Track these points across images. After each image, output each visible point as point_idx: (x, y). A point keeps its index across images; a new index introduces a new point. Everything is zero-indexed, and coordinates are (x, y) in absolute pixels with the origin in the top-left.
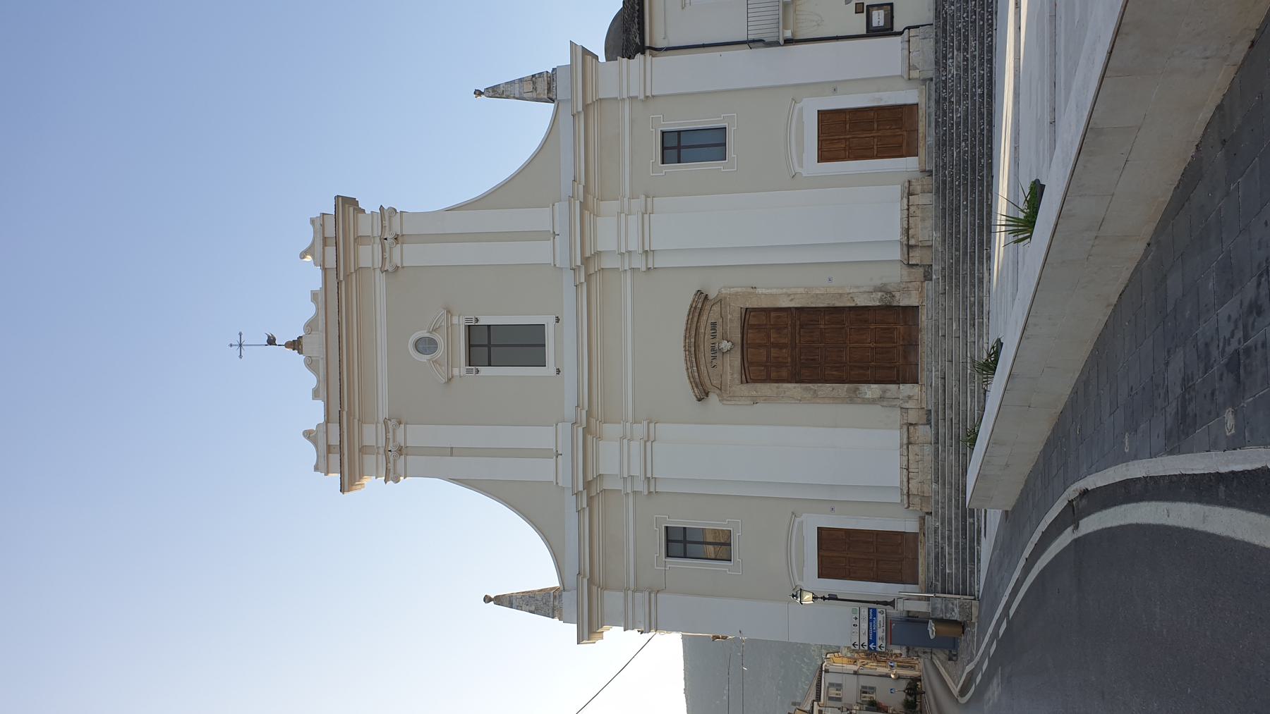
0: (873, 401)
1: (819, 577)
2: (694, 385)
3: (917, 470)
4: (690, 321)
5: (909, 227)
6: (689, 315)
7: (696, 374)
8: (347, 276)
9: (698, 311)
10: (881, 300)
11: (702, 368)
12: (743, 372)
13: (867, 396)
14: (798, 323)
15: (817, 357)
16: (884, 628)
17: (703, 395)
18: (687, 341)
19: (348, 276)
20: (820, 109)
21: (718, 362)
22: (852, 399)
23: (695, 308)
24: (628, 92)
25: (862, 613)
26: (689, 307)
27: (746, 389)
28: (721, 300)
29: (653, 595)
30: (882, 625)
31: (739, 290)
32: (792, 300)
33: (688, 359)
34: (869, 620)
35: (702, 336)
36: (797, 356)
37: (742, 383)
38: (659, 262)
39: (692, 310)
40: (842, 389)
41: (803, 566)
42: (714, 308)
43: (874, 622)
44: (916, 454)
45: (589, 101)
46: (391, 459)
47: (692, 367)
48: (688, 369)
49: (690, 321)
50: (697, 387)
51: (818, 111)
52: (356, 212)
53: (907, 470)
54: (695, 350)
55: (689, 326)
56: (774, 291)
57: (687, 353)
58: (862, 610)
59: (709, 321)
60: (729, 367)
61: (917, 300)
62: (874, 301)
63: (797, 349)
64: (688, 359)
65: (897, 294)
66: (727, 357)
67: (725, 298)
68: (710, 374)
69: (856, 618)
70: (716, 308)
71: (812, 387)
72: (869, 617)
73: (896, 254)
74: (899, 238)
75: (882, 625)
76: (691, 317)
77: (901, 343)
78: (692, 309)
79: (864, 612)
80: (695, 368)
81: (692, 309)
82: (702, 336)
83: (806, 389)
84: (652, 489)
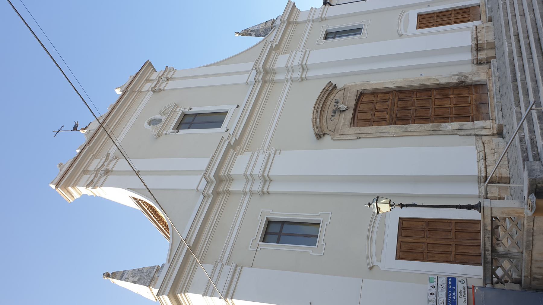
0: (452, 133)
1: (396, 259)
2: (315, 126)
3: (494, 159)
4: (321, 96)
5: (477, 36)
6: (321, 93)
7: (318, 122)
8: (133, 91)
9: (328, 92)
10: (458, 79)
11: (323, 121)
12: (353, 122)
13: (448, 129)
14: (397, 98)
15: (409, 114)
16: (466, 297)
17: (320, 136)
18: (317, 105)
19: (133, 91)
20: (402, 216)
21: (336, 117)
22: (435, 133)
23: (327, 90)
24: (313, 16)
25: (440, 281)
26: (323, 89)
27: (353, 130)
28: (345, 89)
29: (239, 268)
30: (463, 294)
31: (358, 83)
32: (394, 84)
33: (315, 114)
34: (448, 289)
35: (328, 106)
36: (394, 114)
37: (350, 127)
38: (310, 74)
39: (324, 91)
40: (428, 126)
41: (383, 249)
42: (339, 92)
43: (454, 291)
44: (492, 149)
45: (291, 20)
46: (99, 175)
47: (316, 118)
48: (313, 118)
49: (321, 96)
50: (317, 128)
51: (400, 218)
52: (153, 71)
53: (485, 159)
54: (321, 111)
55: (320, 98)
56: (382, 81)
57: (315, 111)
58: (440, 280)
59: (335, 99)
60: (343, 119)
61: (486, 77)
62: (455, 80)
63: (395, 111)
64: (315, 114)
65: (470, 76)
66: (343, 115)
67: (348, 87)
68: (327, 121)
69: (433, 287)
70: (341, 93)
71: (404, 126)
72: (448, 285)
73: (469, 56)
74: (470, 44)
75: (463, 294)
76: (323, 94)
77: (474, 103)
78: (325, 91)
79: (442, 281)
80: (318, 119)
81: (325, 91)
82: (328, 106)
83: (399, 127)
84: (265, 190)
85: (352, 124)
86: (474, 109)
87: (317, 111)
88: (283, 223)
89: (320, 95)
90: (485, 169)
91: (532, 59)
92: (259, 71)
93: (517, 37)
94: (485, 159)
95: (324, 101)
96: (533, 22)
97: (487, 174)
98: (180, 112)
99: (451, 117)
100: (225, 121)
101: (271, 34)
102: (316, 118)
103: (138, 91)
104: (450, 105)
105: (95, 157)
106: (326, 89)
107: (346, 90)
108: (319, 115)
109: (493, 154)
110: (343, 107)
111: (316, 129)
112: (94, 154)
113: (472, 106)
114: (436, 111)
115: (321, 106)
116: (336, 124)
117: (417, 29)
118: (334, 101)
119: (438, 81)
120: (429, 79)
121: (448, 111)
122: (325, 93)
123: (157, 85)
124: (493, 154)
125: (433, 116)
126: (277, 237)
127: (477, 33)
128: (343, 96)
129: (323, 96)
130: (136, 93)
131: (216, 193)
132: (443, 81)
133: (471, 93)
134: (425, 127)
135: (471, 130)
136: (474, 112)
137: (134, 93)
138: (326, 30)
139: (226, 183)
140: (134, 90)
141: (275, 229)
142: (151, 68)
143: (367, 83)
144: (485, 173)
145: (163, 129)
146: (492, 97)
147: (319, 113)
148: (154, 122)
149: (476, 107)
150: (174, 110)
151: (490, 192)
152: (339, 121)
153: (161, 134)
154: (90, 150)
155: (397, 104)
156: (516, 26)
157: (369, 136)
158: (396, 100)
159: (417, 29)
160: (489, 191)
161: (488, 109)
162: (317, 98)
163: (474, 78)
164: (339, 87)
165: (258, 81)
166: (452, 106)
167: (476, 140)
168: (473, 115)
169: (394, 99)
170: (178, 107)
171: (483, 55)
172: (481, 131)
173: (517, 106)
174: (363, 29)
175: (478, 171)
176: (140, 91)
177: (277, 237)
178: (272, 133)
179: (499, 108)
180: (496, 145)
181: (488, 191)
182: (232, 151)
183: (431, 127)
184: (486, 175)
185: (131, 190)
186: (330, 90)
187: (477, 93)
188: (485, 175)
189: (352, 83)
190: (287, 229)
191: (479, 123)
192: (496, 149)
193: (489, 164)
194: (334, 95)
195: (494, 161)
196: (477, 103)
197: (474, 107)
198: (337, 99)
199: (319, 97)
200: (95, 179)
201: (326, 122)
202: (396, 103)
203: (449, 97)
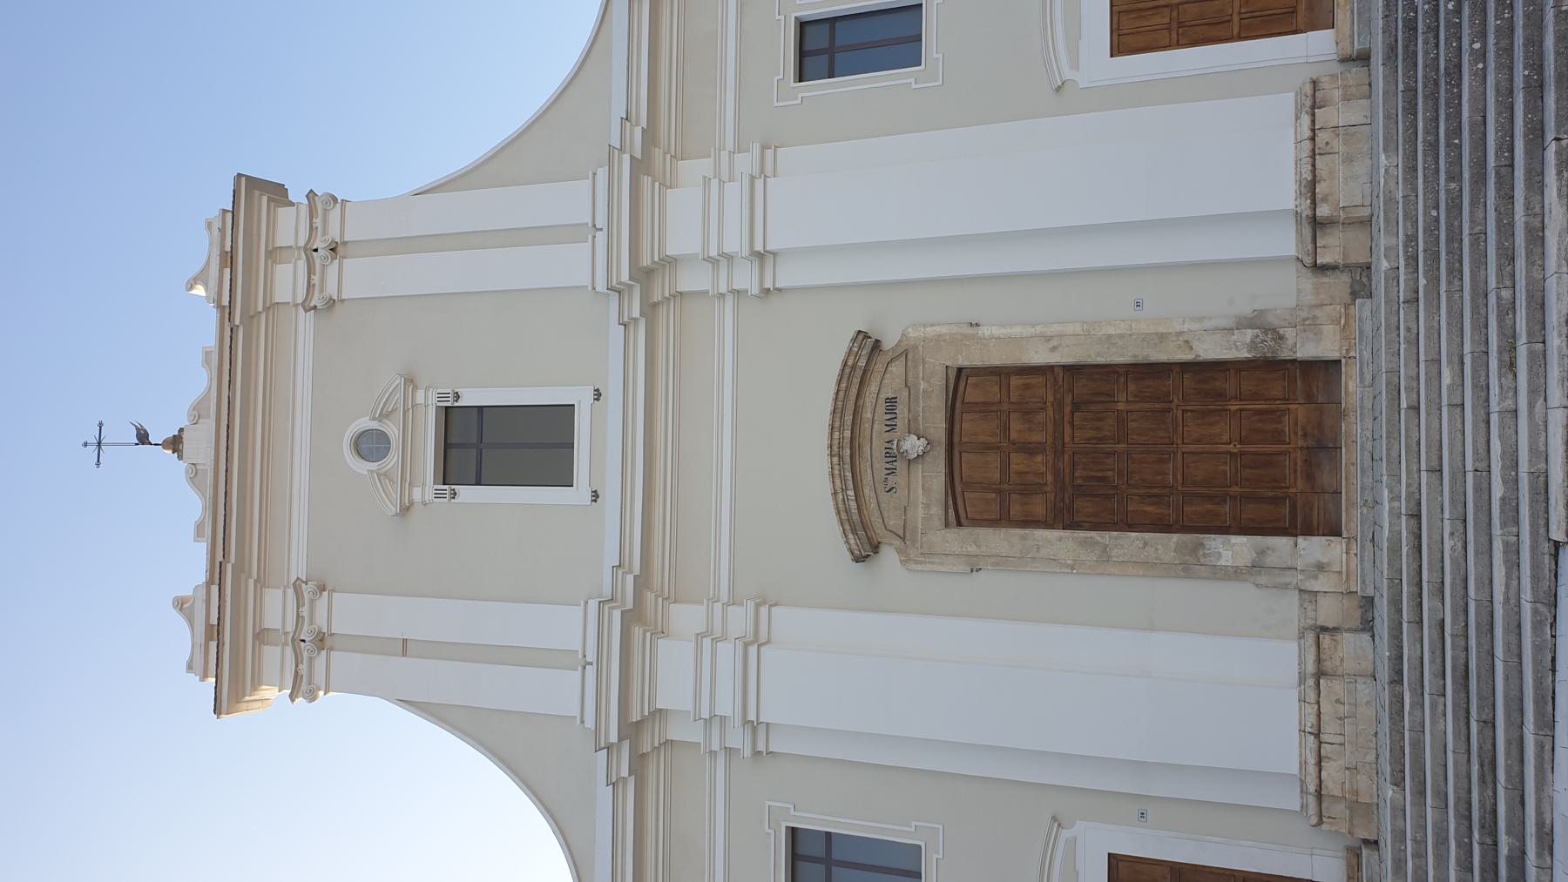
0: (1235, 574)
2: (847, 527)
3: (1339, 739)
8: (250, 318)
9: (859, 373)
10: (1253, 345)
13: (1222, 562)
14: (1068, 399)
17: (866, 549)
18: (836, 434)
19: (252, 317)
21: (899, 480)
22: (1188, 568)
23: (854, 367)
26: (839, 367)
28: (906, 353)
31: (944, 330)
32: (1054, 349)
33: (837, 472)
39: (847, 371)
40: (1167, 544)
44: (1337, 701)
47: (844, 490)
50: (854, 532)
52: (272, 204)
53: (1317, 736)
56: (1017, 331)
57: (836, 459)
63: (1066, 457)
65: (1289, 333)
66: (918, 472)
70: (897, 369)
73: (1286, 242)
78: (847, 370)
80: (851, 493)
84: (761, 747)
85: (950, 511)
86: (1299, 469)
87: (840, 457)
88: (832, 21)
89: (837, 393)
90: (1317, 769)
91: (1442, 699)
92: (627, 563)
93: (1413, 522)
94: (1317, 736)
95: (852, 412)
96: (1457, 581)
97: (1323, 786)
98: (430, 407)
99: (1233, 498)
100: (578, 461)
101: (608, 13)
102: (844, 490)
103: (267, 309)
104: (1230, 443)
105: (261, 584)
106: (850, 362)
107: (910, 356)
108: (849, 474)
109: (1340, 718)
110: (913, 447)
111: (851, 536)
112: (255, 575)
113: (1293, 456)
114: (1188, 468)
115: (848, 434)
116: (905, 507)
117: (1112, 56)
118: (882, 408)
119: (1191, 348)
120: (1162, 337)
121: (1223, 467)
122: (849, 380)
123: (312, 282)
124: (1340, 718)
125: (1179, 488)
126: (824, 58)
127: (1313, 156)
128: (906, 386)
129: (846, 391)
130: (263, 317)
131: (639, 763)
132: (1205, 350)
133: (1292, 397)
134: (1157, 550)
135: (1288, 572)
136: (1300, 484)
137: (255, 320)
138: (796, 18)
139: (654, 723)
140: (252, 314)
141: (818, 40)
142: (260, 200)
143: (970, 331)
144: (1317, 781)
145: (410, 484)
146: (1353, 442)
147: (848, 467)
148: (370, 445)
149: (1306, 460)
150: (410, 407)
151: (1329, 817)
152: (911, 497)
153: (409, 502)
154: (239, 569)
155: (1072, 423)
156: (1415, 468)
157: (1002, 562)
158: (1067, 410)
159: (1112, 56)
160: (1327, 815)
161: (1339, 477)
162: (830, 408)
163: (1301, 347)
164: (889, 343)
165: (622, 287)
166: (1235, 450)
167: (1301, 605)
168: (1295, 494)
169: (1058, 405)
170: (415, 388)
171: (1332, 249)
172: (1316, 577)
173: (1395, 785)
174: (924, 6)
175: (1300, 763)
176: (271, 307)
177: (824, 58)
178: (730, 459)
179: (1366, 532)
180: (1348, 691)
181: (1324, 813)
182: (637, 631)
183: (1175, 551)
184: (1318, 789)
185: (407, 706)
186: (862, 363)
187: (1310, 398)
188: (1316, 791)
189: (925, 326)
190: (844, 35)
191: (1313, 548)
192: (1349, 704)
193: (1330, 755)
194: (879, 380)
195: (1340, 744)
196: (1311, 443)
197: (1299, 462)
198: (890, 396)
199: (836, 399)
200: (300, 666)
201: (873, 494)
202: (1069, 423)
203: (1227, 410)
